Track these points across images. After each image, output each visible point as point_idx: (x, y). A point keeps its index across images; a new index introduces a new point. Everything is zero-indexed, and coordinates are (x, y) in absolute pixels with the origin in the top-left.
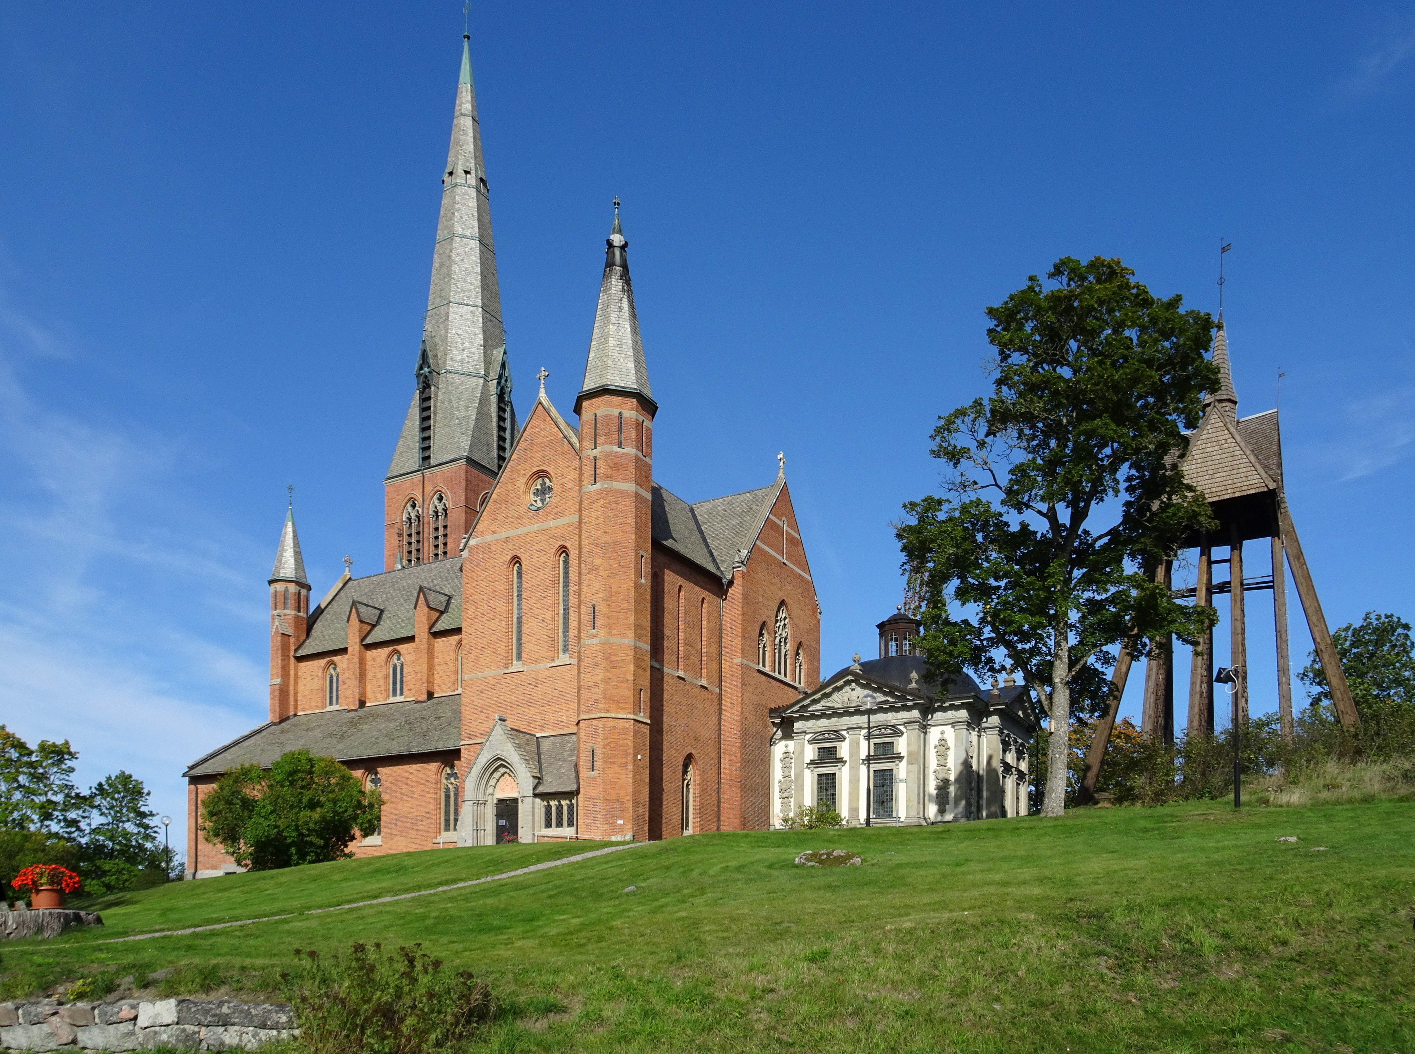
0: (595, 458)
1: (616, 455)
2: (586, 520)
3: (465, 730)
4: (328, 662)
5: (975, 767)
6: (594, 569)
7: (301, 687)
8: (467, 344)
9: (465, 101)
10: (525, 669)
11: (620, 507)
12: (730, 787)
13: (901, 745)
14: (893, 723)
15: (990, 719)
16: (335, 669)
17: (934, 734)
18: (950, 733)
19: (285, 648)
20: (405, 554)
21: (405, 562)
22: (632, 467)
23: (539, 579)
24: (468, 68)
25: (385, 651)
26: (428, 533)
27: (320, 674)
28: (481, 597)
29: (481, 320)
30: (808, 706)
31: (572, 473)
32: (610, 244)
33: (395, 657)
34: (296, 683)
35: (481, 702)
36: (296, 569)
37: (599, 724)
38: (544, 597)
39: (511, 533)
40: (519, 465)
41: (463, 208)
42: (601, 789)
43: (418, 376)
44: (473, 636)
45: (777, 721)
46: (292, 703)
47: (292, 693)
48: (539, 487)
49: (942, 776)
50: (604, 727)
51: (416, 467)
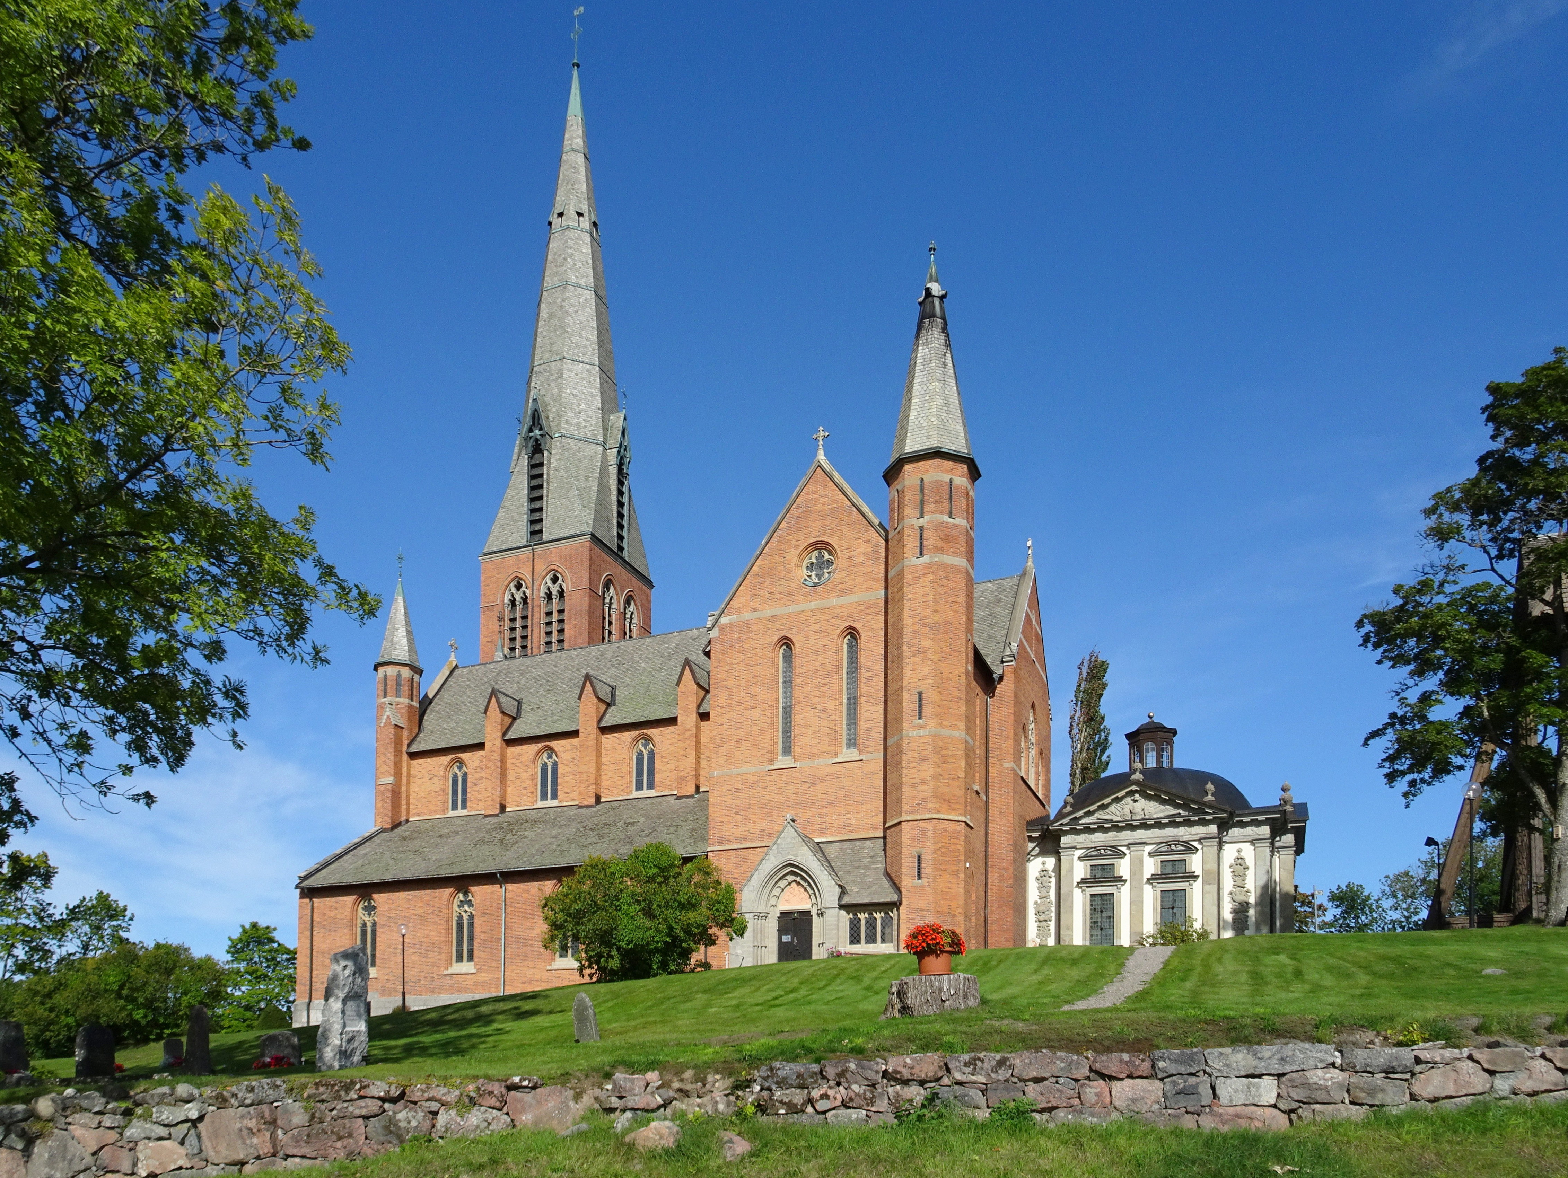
0: (921, 528)
1: (947, 526)
2: (910, 596)
3: (714, 833)
4: (452, 760)
6: (921, 651)
7: (414, 788)
8: (583, 406)
9: (575, 135)
10: (797, 765)
11: (951, 584)
12: (1000, 906)
13: (1195, 863)
14: (1185, 838)
15: (1284, 837)
16: (460, 768)
17: (1230, 852)
18: (1248, 850)
19: (398, 742)
20: (507, 641)
21: (506, 651)
22: (962, 540)
23: (818, 663)
24: (578, 98)
25: (531, 749)
26: (538, 618)
27: (441, 773)
28: (737, 683)
29: (598, 380)
31: (863, 546)
32: (928, 292)
33: (545, 755)
34: (408, 783)
35: (738, 802)
36: (409, 651)
37: (929, 826)
38: (825, 685)
39: (779, 610)
40: (789, 534)
41: (573, 255)
42: (931, 899)
43: (527, 438)
44: (725, 727)
45: (1035, 835)
46: (404, 807)
47: (404, 794)
48: (814, 560)
49: (1241, 898)
50: (935, 829)
51: (524, 542)
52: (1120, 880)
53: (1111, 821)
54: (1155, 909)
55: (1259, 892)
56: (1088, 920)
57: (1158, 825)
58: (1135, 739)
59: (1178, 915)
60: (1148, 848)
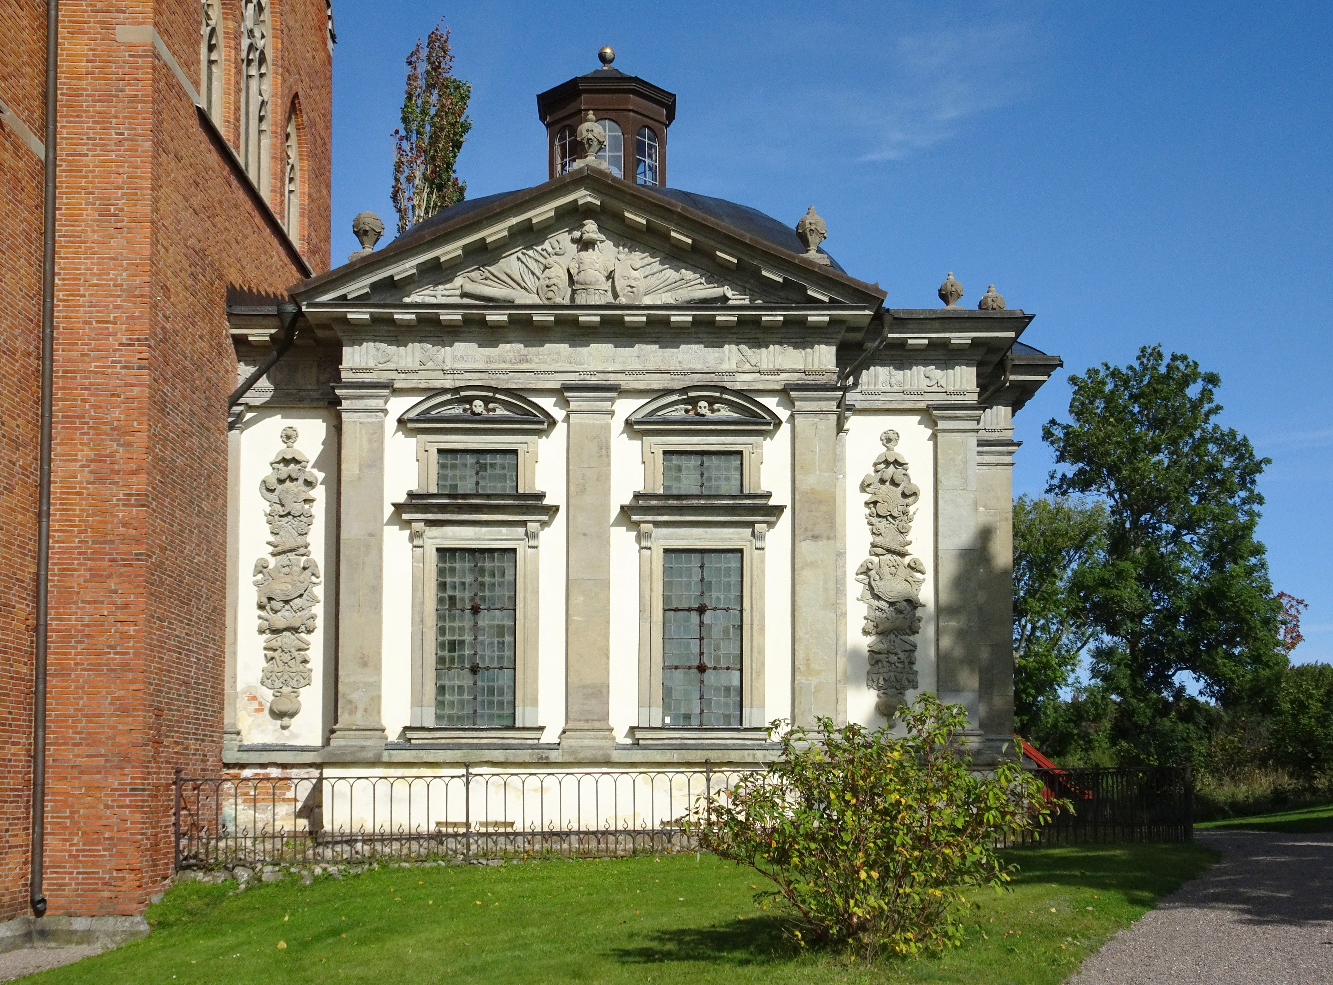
12: (97, 576)
14: (742, 382)
17: (863, 440)
30: (408, 284)
45: (259, 335)
49: (894, 587)
52: (534, 505)
53: (507, 304)
54: (644, 610)
55: (949, 569)
56: (431, 635)
57: (658, 329)
58: (560, 107)
59: (716, 633)
60: (626, 407)
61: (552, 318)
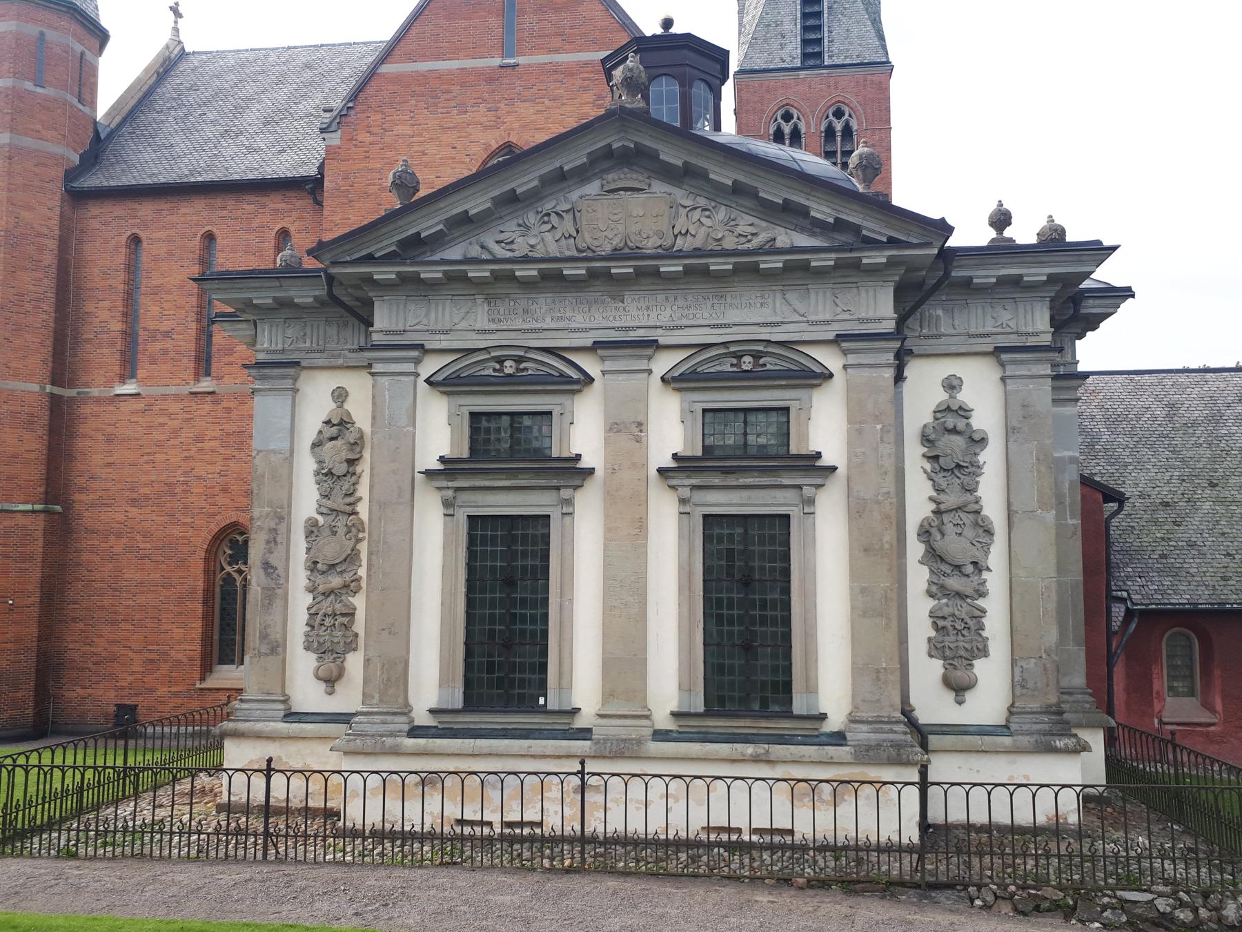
5: (1046, 727)
17: (924, 387)
30: (437, 241)
60: (664, 363)
61: (681, 268)
